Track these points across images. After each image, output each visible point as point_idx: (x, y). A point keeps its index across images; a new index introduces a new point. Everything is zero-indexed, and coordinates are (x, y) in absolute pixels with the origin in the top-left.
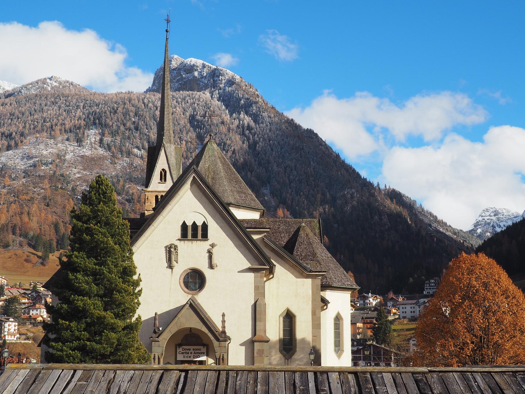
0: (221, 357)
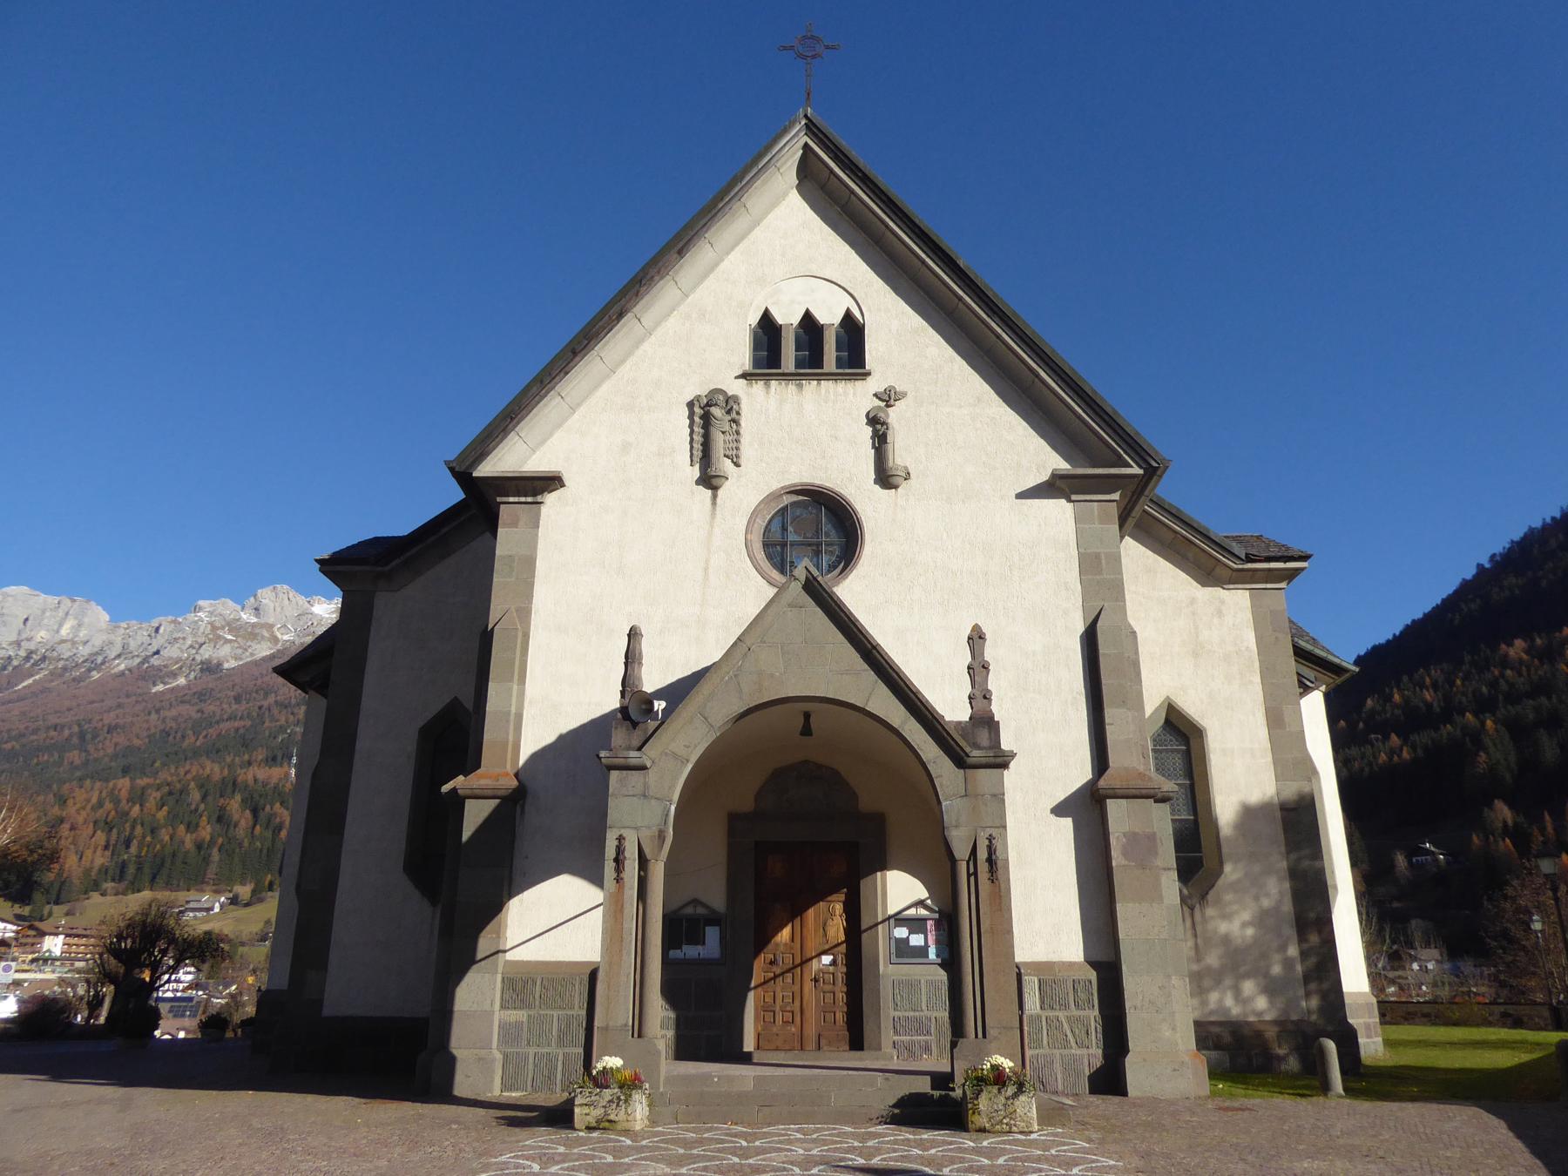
0: (982, 854)
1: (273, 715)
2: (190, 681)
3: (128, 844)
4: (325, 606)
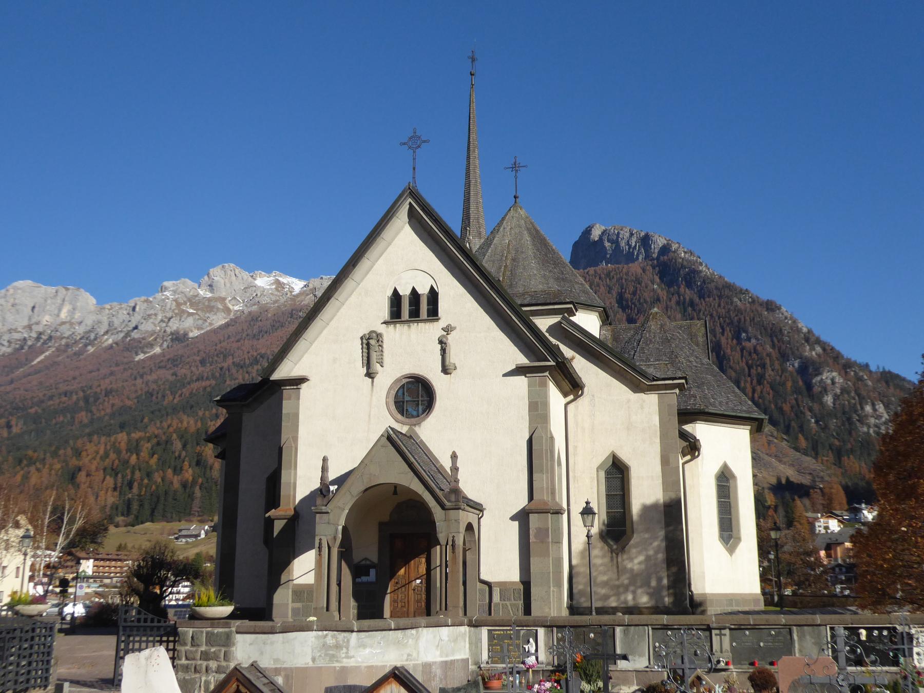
1: (232, 374)
2: (164, 349)
3: (130, 485)
4: (266, 279)
